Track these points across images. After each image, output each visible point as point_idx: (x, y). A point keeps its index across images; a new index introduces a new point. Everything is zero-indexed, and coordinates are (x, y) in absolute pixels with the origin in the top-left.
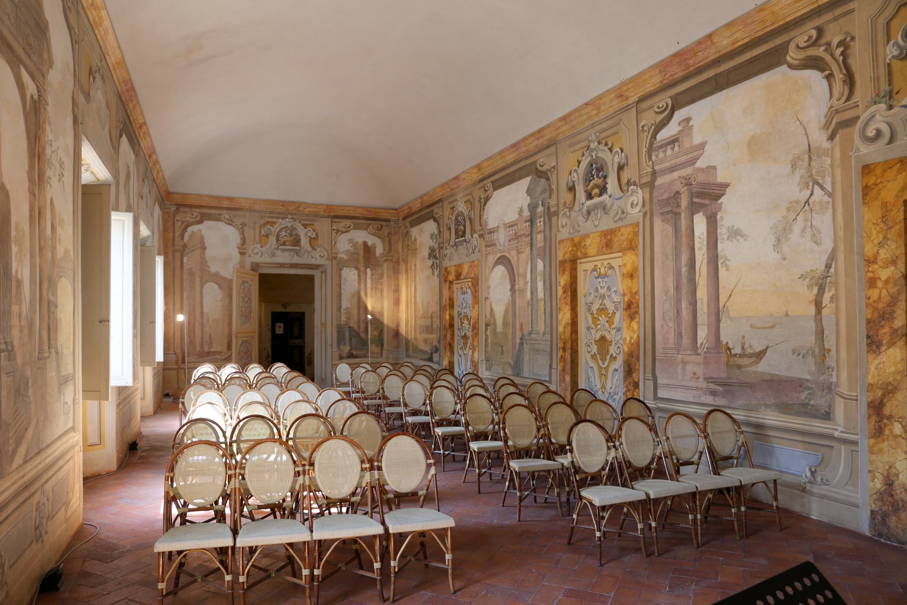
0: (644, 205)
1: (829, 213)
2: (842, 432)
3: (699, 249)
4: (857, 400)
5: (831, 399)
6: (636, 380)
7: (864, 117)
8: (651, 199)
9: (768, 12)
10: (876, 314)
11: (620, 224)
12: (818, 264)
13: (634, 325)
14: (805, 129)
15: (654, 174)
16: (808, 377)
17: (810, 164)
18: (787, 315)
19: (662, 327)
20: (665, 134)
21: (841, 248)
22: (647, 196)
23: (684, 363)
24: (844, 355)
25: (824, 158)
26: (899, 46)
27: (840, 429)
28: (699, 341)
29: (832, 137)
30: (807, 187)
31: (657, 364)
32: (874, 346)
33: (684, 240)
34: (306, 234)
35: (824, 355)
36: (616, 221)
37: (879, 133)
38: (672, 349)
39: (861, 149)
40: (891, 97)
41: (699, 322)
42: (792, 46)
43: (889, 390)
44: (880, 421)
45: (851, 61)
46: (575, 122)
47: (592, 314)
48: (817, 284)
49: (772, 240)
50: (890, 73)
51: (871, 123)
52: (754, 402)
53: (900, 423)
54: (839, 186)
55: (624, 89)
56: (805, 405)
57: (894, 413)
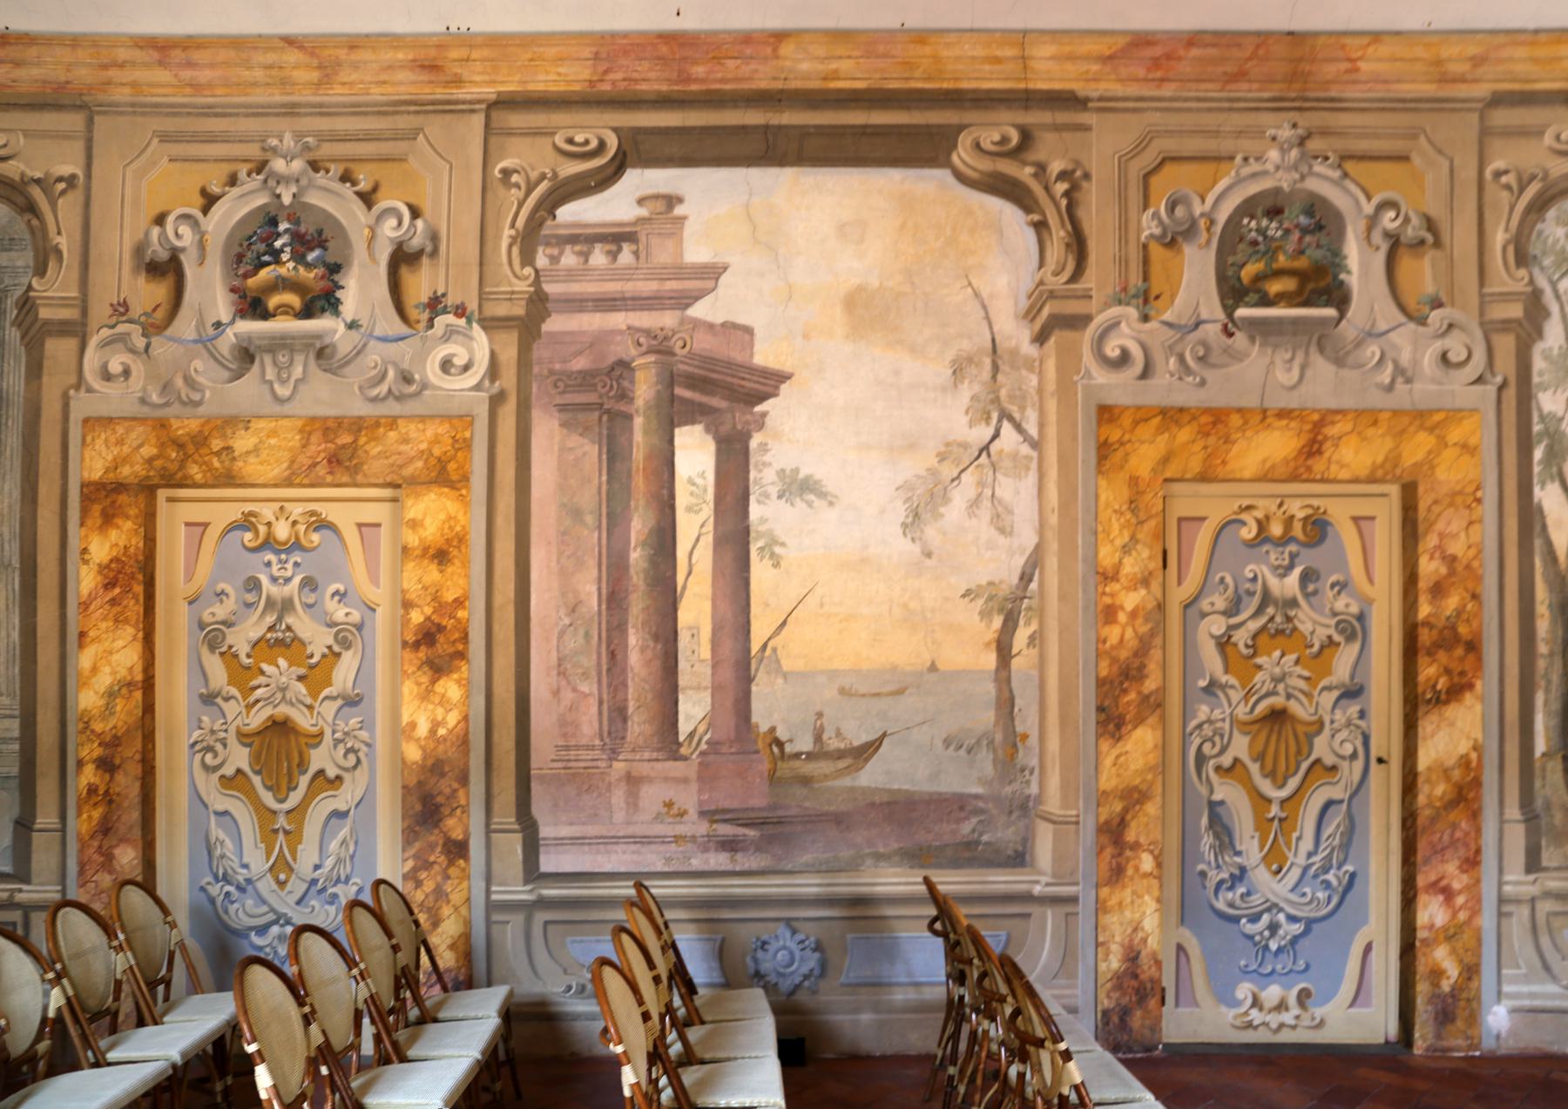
0: (493, 371)
1: (1031, 479)
2: (1048, 884)
3: (689, 509)
4: (1077, 823)
5: (1027, 827)
6: (457, 835)
7: (1099, 320)
9: (927, 50)
10: (1115, 669)
11: (392, 408)
12: (1003, 566)
13: (450, 688)
14: (984, 307)
15: (539, 304)
16: (979, 790)
17: (994, 377)
18: (933, 668)
19: (556, 693)
20: (578, 212)
21: (1053, 546)
22: (509, 354)
23: (633, 782)
24: (1053, 744)
25: (1024, 372)
26: (1161, 222)
27: (1044, 879)
28: (684, 728)
29: (1041, 338)
30: (988, 419)
31: (535, 787)
32: (1111, 726)
33: (639, 483)
34: (1373, 221)
35: (1015, 746)
36: (374, 400)
37: (1124, 358)
38: (592, 748)
39: (1095, 374)
40: (1146, 302)
41: (683, 680)
42: (965, 141)
43: (1134, 797)
44: (1120, 855)
45: (1081, 213)
46: (204, 75)
47: (230, 656)
48: (1000, 610)
49: (900, 512)
50: (1146, 261)
51: (1113, 334)
52: (846, 854)
53: (1151, 852)
54: (1052, 431)
56: (970, 845)
57: (1142, 840)
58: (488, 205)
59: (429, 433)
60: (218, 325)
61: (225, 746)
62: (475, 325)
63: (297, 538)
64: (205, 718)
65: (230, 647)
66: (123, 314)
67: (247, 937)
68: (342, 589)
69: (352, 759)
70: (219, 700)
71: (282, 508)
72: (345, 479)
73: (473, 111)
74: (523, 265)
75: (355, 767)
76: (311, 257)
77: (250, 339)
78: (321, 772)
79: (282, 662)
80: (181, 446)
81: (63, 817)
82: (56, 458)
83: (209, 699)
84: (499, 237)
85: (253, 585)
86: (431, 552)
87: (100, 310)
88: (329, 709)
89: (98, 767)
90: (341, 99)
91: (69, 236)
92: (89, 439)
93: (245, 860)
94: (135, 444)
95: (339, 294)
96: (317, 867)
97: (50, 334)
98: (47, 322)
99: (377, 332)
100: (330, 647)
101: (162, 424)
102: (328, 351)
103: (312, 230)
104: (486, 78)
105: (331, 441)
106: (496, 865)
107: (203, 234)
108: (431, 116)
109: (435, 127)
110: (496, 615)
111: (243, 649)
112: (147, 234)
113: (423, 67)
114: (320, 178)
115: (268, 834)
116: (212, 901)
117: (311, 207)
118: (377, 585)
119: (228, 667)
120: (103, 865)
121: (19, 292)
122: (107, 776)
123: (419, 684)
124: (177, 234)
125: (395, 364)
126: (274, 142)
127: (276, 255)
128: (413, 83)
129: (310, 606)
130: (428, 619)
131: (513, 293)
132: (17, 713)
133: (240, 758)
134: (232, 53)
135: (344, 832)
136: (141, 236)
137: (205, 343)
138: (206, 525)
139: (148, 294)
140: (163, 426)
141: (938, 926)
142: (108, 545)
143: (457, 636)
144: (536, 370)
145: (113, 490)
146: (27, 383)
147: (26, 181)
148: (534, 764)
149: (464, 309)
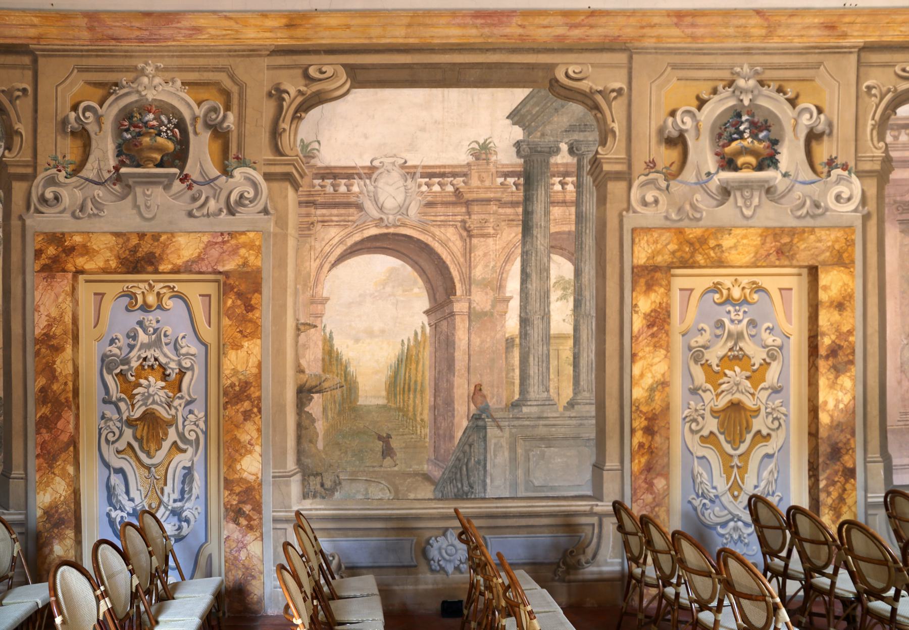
0: (864, 201)
6: (850, 465)
8: (880, 196)
13: (846, 381)
15: (888, 163)
22: (872, 192)
31: (889, 436)
36: (799, 217)
46: (700, 31)
47: (707, 366)
55: (847, 20)
58: (860, 107)
59: (833, 237)
60: (709, 174)
61: (703, 418)
62: (853, 175)
63: (745, 297)
64: (692, 403)
65: (707, 361)
66: (652, 168)
67: (715, 529)
68: (771, 326)
69: (776, 423)
70: (700, 392)
71: (736, 280)
72: (787, 263)
73: (851, 53)
74: (879, 141)
75: (778, 428)
76: (761, 135)
77: (727, 182)
78: (759, 432)
79: (737, 369)
80: (691, 244)
81: (622, 462)
82: (616, 251)
83: (694, 391)
84: (865, 125)
85: (720, 324)
86: (835, 304)
87: (639, 166)
88: (763, 395)
89: (644, 433)
90: (775, 45)
91: (619, 123)
92: (637, 240)
93: (714, 484)
94: (664, 243)
95: (777, 157)
96: (756, 487)
97: (610, 179)
98: (608, 173)
99: (800, 179)
100: (764, 360)
101: (680, 232)
102: (772, 189)
103: (761, 120)
104: (861, 34)
105: (779, 241)
106: (870, 482)
107: (698, 122)
108: (828, 55)
109: (830, 62)
110: (869, 339)
111: (714, 362)
112: (665, 122)
113: (826, 27)
114: (765, 90)
115: (728, 469)
116: (695, 509)
117: (760, 107)
118: (790, 323)
119: (705, 372)
120: (647, 490)
121: (591, 155)
122: (650, 438)
123: (828, 379)
124: (683, 122)
125: (810, 197)
126: (738, 69)
127: (741, 134)
128: (819, 36)
129: (753, 336)
130: (833, 342)
131: (873, 157)
132: (594, 401)
133: (712, 425)
134: (720, 19)
135: (772, 466)
136: (662, 123)
137: (702, 184)
138: (692, 290)
139: (667, 156)
140: (681, 232)
141: (463, 537)
142: (649, 302)
143: (849, 351)
144: (887, 200)
145: (652, 270)
146: (598, 208)
147: (593, 92)
148: (889, 423)
149: (847, 166)
